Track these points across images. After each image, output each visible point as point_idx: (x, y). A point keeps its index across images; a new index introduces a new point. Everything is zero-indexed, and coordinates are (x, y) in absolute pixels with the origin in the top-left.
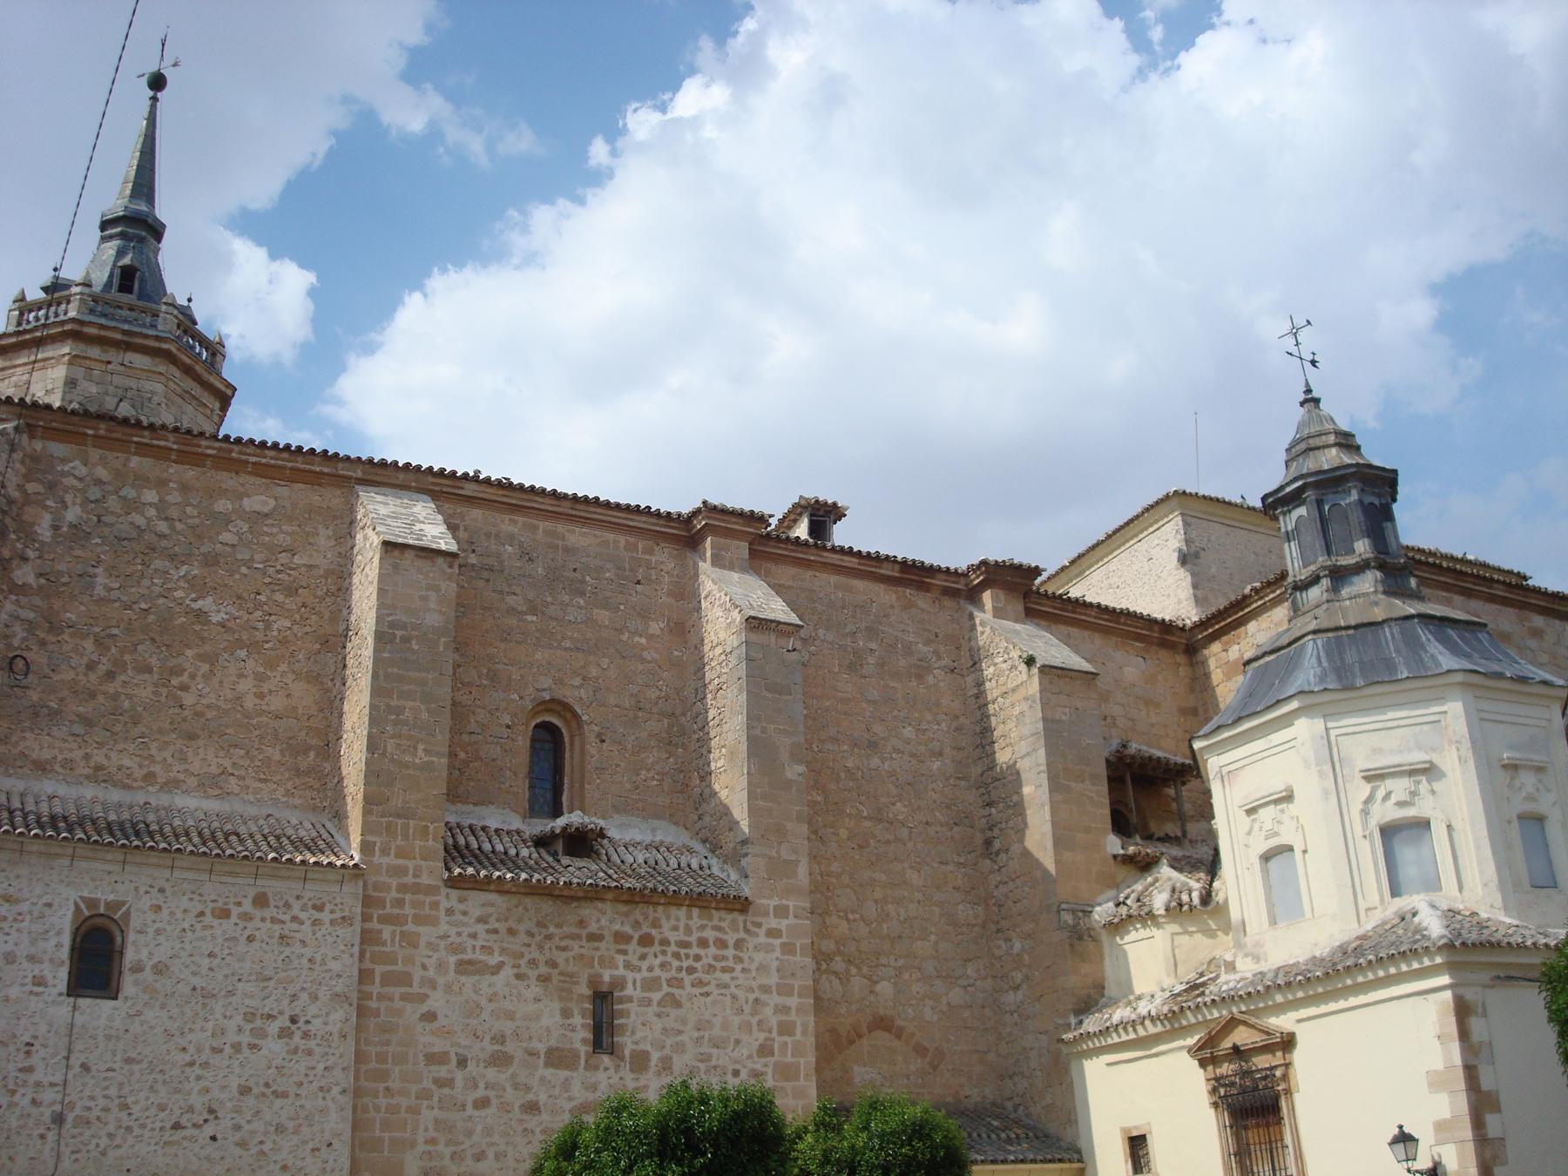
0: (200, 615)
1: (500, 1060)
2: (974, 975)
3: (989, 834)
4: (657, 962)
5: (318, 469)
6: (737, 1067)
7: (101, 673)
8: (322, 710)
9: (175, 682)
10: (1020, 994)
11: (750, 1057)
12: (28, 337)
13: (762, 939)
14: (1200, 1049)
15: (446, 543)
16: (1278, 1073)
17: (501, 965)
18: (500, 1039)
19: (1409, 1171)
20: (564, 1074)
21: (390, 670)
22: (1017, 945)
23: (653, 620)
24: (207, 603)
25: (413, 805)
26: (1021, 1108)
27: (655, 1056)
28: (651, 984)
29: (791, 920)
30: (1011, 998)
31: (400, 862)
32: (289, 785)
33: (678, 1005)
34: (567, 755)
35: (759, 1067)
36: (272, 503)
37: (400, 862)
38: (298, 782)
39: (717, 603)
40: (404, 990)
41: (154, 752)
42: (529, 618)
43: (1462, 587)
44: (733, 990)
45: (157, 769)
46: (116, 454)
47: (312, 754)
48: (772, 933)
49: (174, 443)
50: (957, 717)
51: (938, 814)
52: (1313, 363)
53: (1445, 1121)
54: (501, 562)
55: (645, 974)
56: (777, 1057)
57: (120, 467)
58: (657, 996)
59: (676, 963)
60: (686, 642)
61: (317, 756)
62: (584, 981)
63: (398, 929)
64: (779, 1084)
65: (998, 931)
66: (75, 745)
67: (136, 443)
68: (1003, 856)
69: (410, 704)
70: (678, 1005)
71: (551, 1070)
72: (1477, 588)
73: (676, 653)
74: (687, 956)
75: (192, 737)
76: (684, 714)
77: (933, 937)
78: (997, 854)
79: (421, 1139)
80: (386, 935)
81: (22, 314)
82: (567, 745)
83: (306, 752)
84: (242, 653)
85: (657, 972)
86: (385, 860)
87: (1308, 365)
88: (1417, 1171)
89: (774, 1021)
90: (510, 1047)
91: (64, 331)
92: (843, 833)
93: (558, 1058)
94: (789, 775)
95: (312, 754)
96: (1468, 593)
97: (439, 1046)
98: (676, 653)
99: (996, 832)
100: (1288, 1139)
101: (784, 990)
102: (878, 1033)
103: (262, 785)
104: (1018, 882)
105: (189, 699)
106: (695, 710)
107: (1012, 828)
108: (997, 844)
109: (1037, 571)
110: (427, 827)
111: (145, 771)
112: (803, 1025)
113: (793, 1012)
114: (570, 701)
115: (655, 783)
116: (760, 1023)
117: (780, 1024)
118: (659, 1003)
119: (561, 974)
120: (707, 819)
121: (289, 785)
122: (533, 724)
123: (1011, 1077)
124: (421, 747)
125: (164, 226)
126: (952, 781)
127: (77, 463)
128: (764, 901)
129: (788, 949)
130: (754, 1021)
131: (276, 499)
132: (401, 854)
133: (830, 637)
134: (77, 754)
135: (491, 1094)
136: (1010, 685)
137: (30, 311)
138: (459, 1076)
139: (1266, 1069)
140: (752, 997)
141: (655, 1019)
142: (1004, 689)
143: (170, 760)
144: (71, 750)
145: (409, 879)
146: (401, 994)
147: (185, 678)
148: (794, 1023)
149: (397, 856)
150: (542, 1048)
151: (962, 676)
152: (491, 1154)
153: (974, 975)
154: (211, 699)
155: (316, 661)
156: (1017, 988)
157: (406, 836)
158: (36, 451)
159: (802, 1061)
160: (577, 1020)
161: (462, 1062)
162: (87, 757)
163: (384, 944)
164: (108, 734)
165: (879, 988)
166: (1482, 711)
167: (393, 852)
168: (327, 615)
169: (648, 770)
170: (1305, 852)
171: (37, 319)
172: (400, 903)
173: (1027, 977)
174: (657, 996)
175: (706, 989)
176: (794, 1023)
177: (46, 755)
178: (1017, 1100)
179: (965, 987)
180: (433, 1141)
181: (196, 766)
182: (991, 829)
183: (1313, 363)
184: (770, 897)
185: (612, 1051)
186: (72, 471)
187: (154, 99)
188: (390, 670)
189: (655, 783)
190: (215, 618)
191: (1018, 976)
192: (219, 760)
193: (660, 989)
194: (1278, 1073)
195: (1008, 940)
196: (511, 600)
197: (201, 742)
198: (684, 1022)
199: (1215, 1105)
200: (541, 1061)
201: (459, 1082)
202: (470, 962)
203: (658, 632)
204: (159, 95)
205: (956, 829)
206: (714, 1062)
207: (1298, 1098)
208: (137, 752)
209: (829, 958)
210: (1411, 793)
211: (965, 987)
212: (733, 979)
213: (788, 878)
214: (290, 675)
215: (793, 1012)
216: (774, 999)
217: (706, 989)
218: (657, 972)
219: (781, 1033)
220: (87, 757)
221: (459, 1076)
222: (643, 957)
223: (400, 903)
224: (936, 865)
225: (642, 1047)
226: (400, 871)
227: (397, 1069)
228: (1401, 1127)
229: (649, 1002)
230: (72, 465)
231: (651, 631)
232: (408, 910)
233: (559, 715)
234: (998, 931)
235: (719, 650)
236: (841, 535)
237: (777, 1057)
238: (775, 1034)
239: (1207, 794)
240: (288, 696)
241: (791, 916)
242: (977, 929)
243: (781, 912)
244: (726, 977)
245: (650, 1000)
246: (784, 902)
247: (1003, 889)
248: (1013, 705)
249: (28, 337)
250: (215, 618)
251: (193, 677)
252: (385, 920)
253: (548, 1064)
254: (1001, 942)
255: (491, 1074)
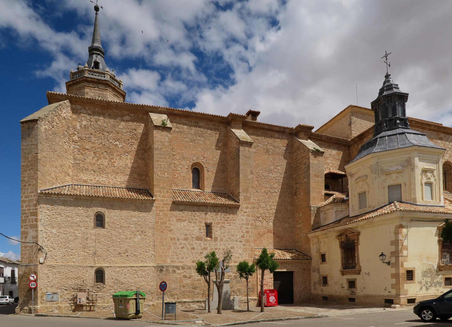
0: (116, 145)
1: (185, 239)
2: (291, 221)
3: (296, 190)
4: (219, 219)
5: (139, 109)
6: (237, 240)
7: (95, 160)
8: (145, 166)
9: (112, 161)
10: (301, 225)
11: (240, 238)
12: (75, 82)
13: (242, 214)
14: (338, 236)
15: (169, 125)
16: (355, 241)
17: (185, 220)
18: (186, 235)
19: (383, 262)
20: (200, 242)
21: (158, 156)
22: (301, 215)
23: (219, 143)
24: (117, 143)
25: (165, 186)
26: (299, 249)
27: (219, 238)
28: (218, 223)
29: (249, 209)
30: (298, 226)
31: (163, 199)
32: (140, 183)
33: (224, 228)
34: (201, 175)
35: (241, 240)
36: (130, 118)
37: (163, 199)
38: (141, 182)
39: (234, 138)
40: (165, 225)
41: (109, 177)
42: (191, 143)
43: (423, 127)
44: (236, 224)
45: (110, 180)
46: (92, 107)
47: (144, 176)
48: (245, 212)
49: (105, 104)
50: (291, 164)
51: (285, 186)
52: (389, 65)
53: (393, 252)
54: (184, 130)
55: (217, 221)
56: (245, 238)
57: (94, 111)
58: (219, 226)
59: (223, 219)
60: (227, 148)
61: (145, 176)
62: (203, 223)
63: (163, 213)
64: (246, 244)
65: (297, 212)
66: (92, 176)
67: (96, 104)
68: (299, 195)
69: (163, 164)
70: (224, 228)
71: (197, 241)
72: (426, 127)
73: (225, 151)
74: (226, 218)
75: (118, 173)
76: (227, 165)
77: (282, 213)
78: (298, 195)
79: (170, 255)
80: (161, 214)
81: (73, 76)
82: (200, 173)
83: (143, 175)
84: (127, 154)
85: (219, 221)
86: (159, 198)
87: (388, 66)
88: (385, 262)
89: (245, 231)
90: (188, 236)
91: (83, 80)
92: (263, 191)
93: (198, 239)
94: (249, 178)
95: (144, 176)
96: (423, 128)
97: (173, 236)
98: (225, 151)
99: (298, 190)
100: (356, 255)
101: (247, 224)
102: (269, 233)
103: (134, 183)
104: (302, 201)
105: (116, 165)
106: (229, 163)
107: (301, 189)
108: (298, 193)
109: (312, 128)
110: (168, 191)
111: (108, 181)
112: (251, 231)
113: (249, 229)
114: (201, 162)
115: (220, 180)
116: (242, 231)
117: (246, 231)
118: (220, 227)
119: (199, 221)
120: (231, 188)
121: (140, 183)
122: (193, 168)
123: (298, 242)
124: (166, 173)
125: (371, 103)
126: (288, 179)
127: (83, 110)
128: (243, 205)
129: (248, 216)
130: (241, 231)
131: (131, 117)
132: (163, 197)
133: (261, 146)
134: (93, 178)
135: (184, 246)
136: (303, 156)
137: (75, 75)
138: (178, 242)
139: (353, 240)
140: (240, 226)
141: (219, 230)
142: (302, 157)
143: (113, 179)
144: (91, 177)
145: (165, 202)
146: (24, 246)
147: (114, 160)
148: (249, 231)
149: (162, 197)
150: (195, 236)
151: (293, 154)
152: (185, 258)
153: (291, 221)
154: (121, 164)
155: (143, 155)
156: (300, 224)
157: (164, 193)
158: (73, 107)
159: (251, 239)
160: (202, 231)
161: (178, 240)
162: (95, 178)
163: (160, 216)
164: (99, 173)
165: (269, 224)
166: (420, 156)
167: (161, 197)
168: (145, 145)
169: (219, 178)
170: (368, 192)
171: (76, 77)
172: (163, 207)
173: (302, 221)
174: (219, 226)
175: (230, 224)
176: (249, 231)
177: (86, 178)
178: (298, 247)
179: (288, 224)
180: (173, 255)
181: (119, 180)
182: (297, 189)
183: (389, 65)
184: (245, 205)
185: (211, 237)
186: (83, 112)
187: (96, 14)
188: (158, 156)
189: (220, 180)
190: (120, 146)
191: (301, 221)
192: (124, 178)
193: (220, 224)
194: (355, 241)
195: (299, 214)
196: (186, 139)
197: (119, 174)
198: (225, 231)
199: (340, 248)
200: (195, 239)
201: (178, 244)
202: (179, 219)
203: (221, 146)
204: (98, 12)
205: (289, 189)
206: (232, 239)
207: (360, 247)
208: (106, 177)
209: (258, 217)
210: (427, 176)
211: (288, 224)
212: (236, 222)
213: (249, 200)
214: (138, 159)
215: (249, 229)
216: (245, 226)
217: (230, 224)
218: (219, 221)
219: (246, 233)
220: (95, 178)
221: (178, 242)
222: (216, 218)
223: (163, 207)
224: (283, 198)
225: (216, 236)
226: (163, 201)
227: (165, 241)
228: (382, 253)
229: (218, 227)
230: (82, 110)
231: (219, 145)
232: (165, 209)
233: (198, 166)
234: (297, 212)
235: (234, 149)
236: (259, 119)
237: (245, 238)
238: (245, 233)
239: (347, 180)
240: (138, 163)
241: (249, 209)
242: (292, 211)
243: (247, 208)
244: (234, 222)
245: (218, 227)
246: (248, 206)
247: (298, 203)
248: (303, 161)
249: (75, 82)
250: (120, 146)
251: (116, 159)
252: (160, 211)
253: (196, 240)
254: (297, 214)
255: (184, 242)
